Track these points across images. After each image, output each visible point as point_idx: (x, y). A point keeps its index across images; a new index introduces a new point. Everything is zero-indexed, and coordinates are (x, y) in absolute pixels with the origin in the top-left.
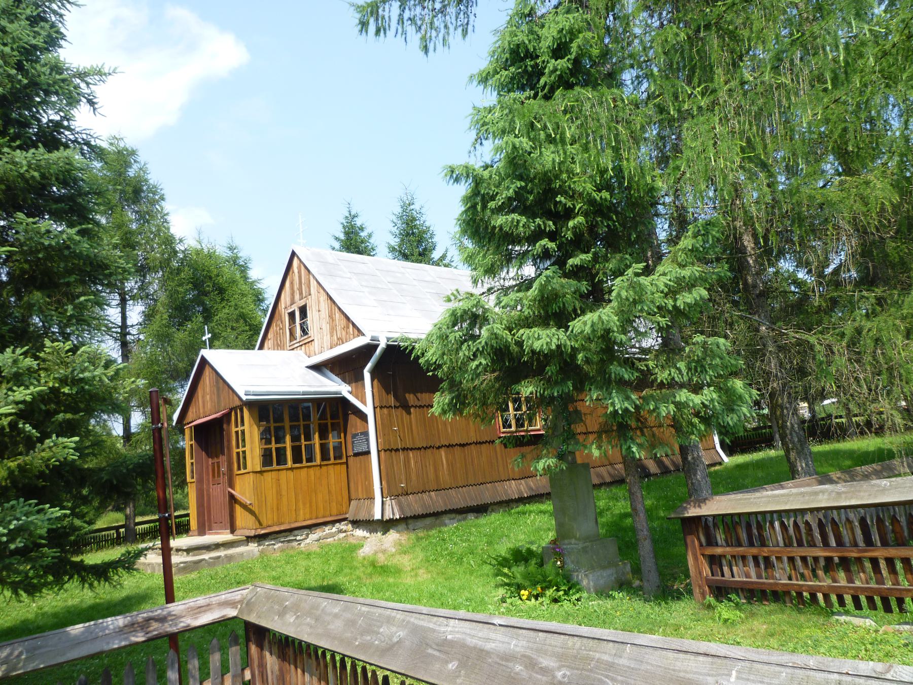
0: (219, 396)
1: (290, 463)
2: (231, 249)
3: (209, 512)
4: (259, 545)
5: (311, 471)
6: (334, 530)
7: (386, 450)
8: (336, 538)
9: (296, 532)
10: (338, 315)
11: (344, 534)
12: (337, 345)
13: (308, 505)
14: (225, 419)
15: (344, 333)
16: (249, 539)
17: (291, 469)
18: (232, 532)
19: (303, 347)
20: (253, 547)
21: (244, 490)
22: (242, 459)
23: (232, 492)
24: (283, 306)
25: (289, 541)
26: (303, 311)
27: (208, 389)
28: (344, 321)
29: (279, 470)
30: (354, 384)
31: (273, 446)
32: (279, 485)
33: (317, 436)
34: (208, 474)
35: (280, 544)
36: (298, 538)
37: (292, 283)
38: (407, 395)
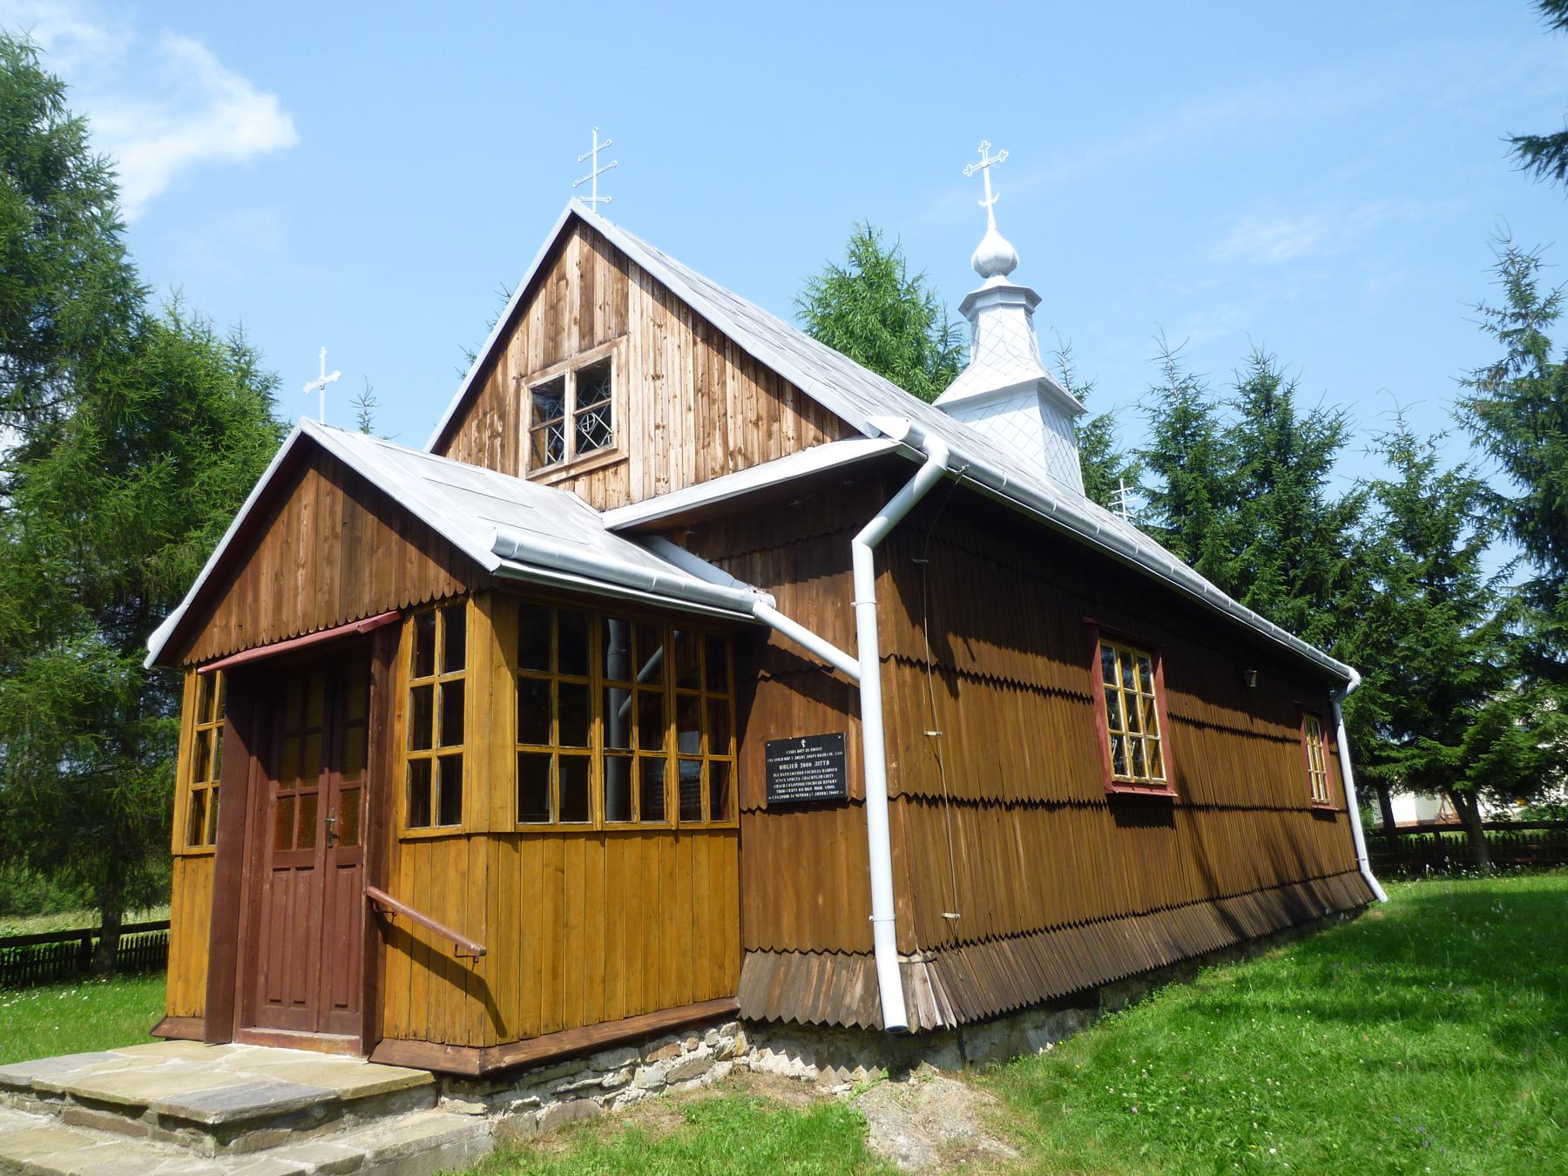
0: (351, 568)
1: (598, 817)
2: (238, 352)
3: (252, 959)
4: (493, 1109)
5: (655, 848)
6: (703, 1050)
8: (707, 1078)
9: (603, 1059)
10: (735, 383)
11: (727, 1065)
12: (724, 470)
13: (639, 964)
14: (378, 644)
15: (756, 437)
16: (448, 1082)
18: (370, 1045)
19: (581, 484)
20: (457, 1118)
21: (438, 890)
22: (442, 793)
23: (376, 893)
24: (513, 371)
25: (581, 1093)
26: (594, 382)
27: (303, 551)
29: (565, 836)
30: (787, 588)
31: (554, 748)
32: (560, 890)
33: (673, 727)
34: (261, 833)
35: (554, 1105)
36: (608, 1079)
37: (554, 309)
38: (951, 637)
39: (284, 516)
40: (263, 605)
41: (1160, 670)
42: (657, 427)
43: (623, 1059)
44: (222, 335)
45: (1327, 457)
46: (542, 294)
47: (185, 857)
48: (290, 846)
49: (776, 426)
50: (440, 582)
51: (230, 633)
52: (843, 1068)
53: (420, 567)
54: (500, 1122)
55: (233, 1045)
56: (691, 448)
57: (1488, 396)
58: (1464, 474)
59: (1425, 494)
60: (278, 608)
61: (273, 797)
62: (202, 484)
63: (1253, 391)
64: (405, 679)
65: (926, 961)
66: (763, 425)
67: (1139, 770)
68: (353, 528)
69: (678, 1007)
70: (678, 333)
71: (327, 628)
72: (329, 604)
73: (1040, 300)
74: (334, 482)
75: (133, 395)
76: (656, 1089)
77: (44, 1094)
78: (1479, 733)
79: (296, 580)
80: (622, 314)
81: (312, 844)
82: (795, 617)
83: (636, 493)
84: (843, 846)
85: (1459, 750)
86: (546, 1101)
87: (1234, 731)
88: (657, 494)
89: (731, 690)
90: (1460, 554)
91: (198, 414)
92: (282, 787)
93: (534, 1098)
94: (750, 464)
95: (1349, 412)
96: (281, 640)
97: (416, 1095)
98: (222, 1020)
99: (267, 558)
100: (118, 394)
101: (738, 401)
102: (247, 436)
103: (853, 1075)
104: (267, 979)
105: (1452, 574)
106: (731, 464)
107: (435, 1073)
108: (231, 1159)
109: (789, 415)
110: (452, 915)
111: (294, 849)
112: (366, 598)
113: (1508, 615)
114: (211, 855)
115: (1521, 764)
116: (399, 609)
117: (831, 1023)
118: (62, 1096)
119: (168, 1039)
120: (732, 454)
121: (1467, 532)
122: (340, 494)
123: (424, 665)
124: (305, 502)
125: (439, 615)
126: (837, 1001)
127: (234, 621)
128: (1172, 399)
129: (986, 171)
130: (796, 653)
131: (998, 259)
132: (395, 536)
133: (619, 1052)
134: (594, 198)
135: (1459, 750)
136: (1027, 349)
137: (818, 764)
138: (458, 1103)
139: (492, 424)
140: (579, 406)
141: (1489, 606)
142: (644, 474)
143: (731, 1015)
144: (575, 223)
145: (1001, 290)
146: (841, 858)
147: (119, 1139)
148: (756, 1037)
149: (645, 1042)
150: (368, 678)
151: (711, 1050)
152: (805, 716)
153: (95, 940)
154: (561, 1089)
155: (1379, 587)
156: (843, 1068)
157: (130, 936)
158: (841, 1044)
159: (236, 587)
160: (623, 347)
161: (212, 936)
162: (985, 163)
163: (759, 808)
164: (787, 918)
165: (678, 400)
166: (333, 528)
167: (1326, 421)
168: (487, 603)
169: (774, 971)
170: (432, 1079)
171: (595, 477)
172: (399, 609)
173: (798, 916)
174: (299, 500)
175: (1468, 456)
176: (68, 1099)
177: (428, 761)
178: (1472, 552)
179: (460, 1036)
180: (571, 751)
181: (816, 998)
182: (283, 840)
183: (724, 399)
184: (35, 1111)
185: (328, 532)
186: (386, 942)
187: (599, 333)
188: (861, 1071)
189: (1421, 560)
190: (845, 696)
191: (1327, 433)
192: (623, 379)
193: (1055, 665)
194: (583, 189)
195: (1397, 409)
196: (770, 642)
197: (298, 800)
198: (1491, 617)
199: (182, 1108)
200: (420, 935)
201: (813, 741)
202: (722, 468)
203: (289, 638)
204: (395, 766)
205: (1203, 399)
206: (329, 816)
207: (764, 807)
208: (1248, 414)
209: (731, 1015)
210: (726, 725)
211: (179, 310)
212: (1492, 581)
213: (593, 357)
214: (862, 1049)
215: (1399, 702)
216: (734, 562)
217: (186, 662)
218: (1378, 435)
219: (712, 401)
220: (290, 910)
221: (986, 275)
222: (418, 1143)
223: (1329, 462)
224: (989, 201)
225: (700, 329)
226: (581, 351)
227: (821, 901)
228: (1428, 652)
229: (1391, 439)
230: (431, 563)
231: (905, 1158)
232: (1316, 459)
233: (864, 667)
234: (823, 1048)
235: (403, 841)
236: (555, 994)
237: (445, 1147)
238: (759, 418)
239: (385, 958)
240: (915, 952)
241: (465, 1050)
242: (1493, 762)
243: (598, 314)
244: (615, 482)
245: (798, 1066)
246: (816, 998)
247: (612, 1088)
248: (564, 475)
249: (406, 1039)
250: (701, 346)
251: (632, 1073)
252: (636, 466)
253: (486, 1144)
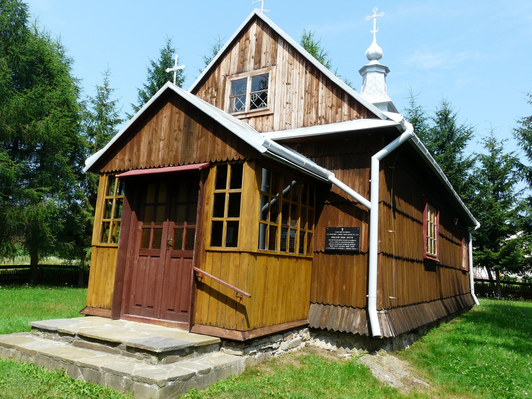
0: (187, 143)
1: (278, 251)
3: (129, 289)
4: (245, 354)
7: (383, 254)
8: (299, 348)
9: (274, 338)
10: (323, 90)
12: (316, 123)
13: (284, 305)
15: (330, 113)
16: (228, 343)
17: (277, 256)
19: (252, 121)
24: (223, 73)
26: (262, 83)
28: (333, 99)
34: (135, 241)
35: (259, 354)
36: (274, 346)
37: (243, 51)
39: (154, 119)
40: (142, 153)
41: (438, 216)
42: (287, 103)
43: (279, 339)
44: (54, 38)
45: (465, 143)
46: (238, 45)
47: (97, 247)
48: (148, 247)
49: (340, 110)
50: (232, 153)
51: (125, 163)
52: (347, 348)
53: (222, 147)
54: (247, 359)
55: (120, 320)
56: (302, 114)
57: (525, 128)
58: (513, 155)
59: (497, 161)
60: (149, 155)
61: (140, 228)
62: (48, 98)
63: (441, 115)
64: (210, 189)
65: (386, 313)
66: (334, 109)
67: (292, 250)
68: (189, 128)
69: (293, 321)
70: (299, 68)
71: (174, 166)
73: (389, 71)
74: (180, 108)
75: (22, 57)
76: (286, 350)
77: (63, 334)
78: (506, 249)
79: (159, 145)
80: (274, 57)
81: (159, 247)
82: (342, 181)
83: (276, 126)
84: (355, 269)
85: (497, 254)
86: (258, 352)
87: (446, 238)
88: (285, 129)
89: (315, 206)
90: (507, 184)
91: (44, 70)
92: (144, 225)
93: (255, 351)
94: (327, 122)
95: (475, 128)
96: (150, 168)
97: (214, 346)
98: (118, 309)
99: (145, 135)
100: (17, 56)
101: (324, 98)
102: (63, 81)
103: (352, 351)
104: (134, 297)
105: (502, 191)
106: (319, 122)
107: (222, 339)
108: (162, 366)
109: (345, 107)
110: (231, 281)
111: (150, 248)
112: (195, 156)
113: (521, 207)
114: (117, 247)
115: (520, 262)
116: (211, 162)
117: (348, 332)
118: (73, 336)
119: (87, 315)
120: (319, 118)
121: (510, 176)
122: (183, 114)
123: (220, 183)
124: (165, 115)
125: (229, 167)
126: (350, 324)
127: (127, 158)
128: (411, 114)
129: (375, 19)
130: (342, 195)
131: (377, 54)
132: (210, 134)
133: (278, 336)
134: (262, 10)
135: (497, 254)
136: (384, 90)
137: (348, 238)
138: (230, 350)
139: (212, 92)
141: (514, 204)
142: (280, 120)
143: (306, 326)
144: (256, 19)
145: (377, 66)
146: (355, 273)
147: (105, 354)
148: (313, 334)
149: (284, 333)
150: (198, 188)
151: (301, 338)
152: (343, 219)
154: (262, 348)
155: (477, 193)
156: (347, 348)
158: (347, 340)
159: (128, 144)
160: (274, 70)
161: (116, 278)
162: (375, 16)
163: (321, 251)
164: (330, 292)
165: (297, 94)
166: (179, 127)
167: (466, 129)
168: (254, 165)
169: (323, 311)
170: (220, 341)
171: (258, 119)
172: (211, 162)
173: (334, 293)
174: (162, 114)
175: (513, 148)
176: (76, 337)
177: (222, 222)
178: (510, 184)
179: (232, 325)
180: (273, 224)
181: (341, 322)
182: (145, 244)
183: (318, 96)
184: (58, 340)
185: (176, 128)
186: (198, 288)
187: (263, 63)
188: (355, 350)
189: (492, 184)
190: (364, 215)
191: (466, 134)
192: (273, 83)
193: (416, 210)
194: (258, 5)
195: (487, 130)
196: (331, 190)
198: (514, 208)
199: (142, 345)
200: (215, 287)
201: (346, 229)
202: (315, 123)
203: (154, 167)
204: (205, 223)
205: (424, 116)
206: (167, 237)
207: (323, 251)
208: (437, 123)
209: (306, 326)
210: (312, 218)
211: (37, 26)
212: (516, 195)
213: (261, 72)
214: (355, 342)
215: (479, 234)
216: (317, 159)
217: (102, 171)
218: (483, 137)
219: (312, 96)
221: (370, 59)
222: (226, 364)
223: (465, 145)
224: (375, 31)
225: (309, 68)
226: (255, 69)
227: (344, 287)
228: (492, 218)
229: (487, 139)
230: (228, 146)
231: (392, 383)
232: (460, 143)
233: (373, 205)
234: (340, 341)
235: (206, 251)
236: (263, 313)
237: (232, 366)
238: (332, 106)
239: (197, 294)
240: (382, 310)
241: (235, 332)
242: (510, 260)
243: (263, 56)
244: (267, 122)
245: (329, 346)
246: (341, 322)
247: (275, 349)
248: (244, 116)
249: (206, 325)
250: (309, 75)
251: (280, 343)
252: (277, 117)
253: (243, 366)
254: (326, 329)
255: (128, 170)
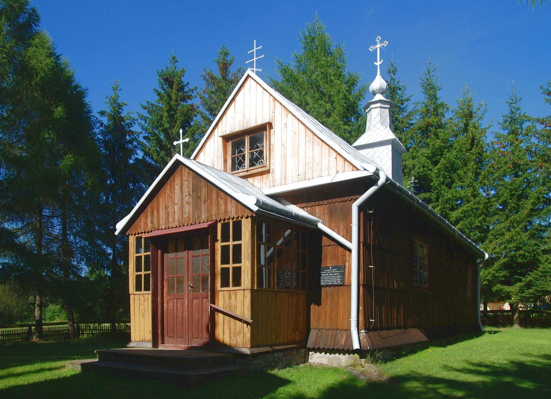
40: (161, 216)
72: (189, 217)
112: (203, 216)
140: (250, 150)
153: (33, 328)
157: (46, 327)
166: (189, 192)
185: (187, 194)
190: (350, 251)
197: (175, 278)
220: (175, 311)
227: (333, 315)
254: (319, 348)
255: (152, 231)
